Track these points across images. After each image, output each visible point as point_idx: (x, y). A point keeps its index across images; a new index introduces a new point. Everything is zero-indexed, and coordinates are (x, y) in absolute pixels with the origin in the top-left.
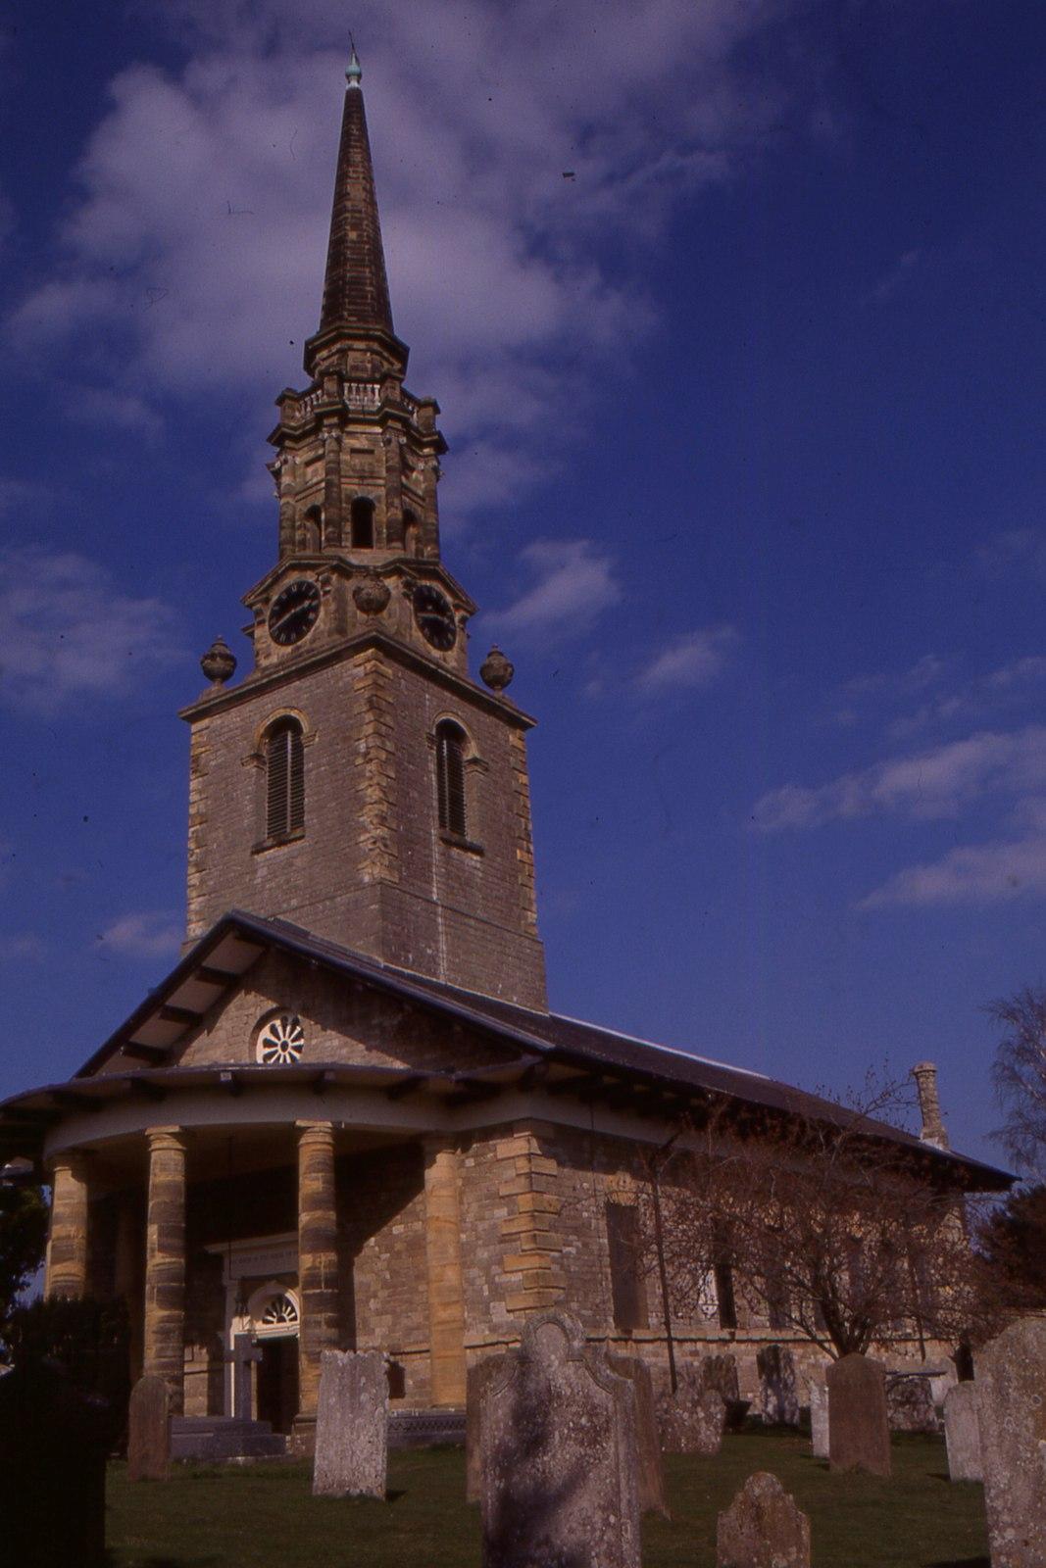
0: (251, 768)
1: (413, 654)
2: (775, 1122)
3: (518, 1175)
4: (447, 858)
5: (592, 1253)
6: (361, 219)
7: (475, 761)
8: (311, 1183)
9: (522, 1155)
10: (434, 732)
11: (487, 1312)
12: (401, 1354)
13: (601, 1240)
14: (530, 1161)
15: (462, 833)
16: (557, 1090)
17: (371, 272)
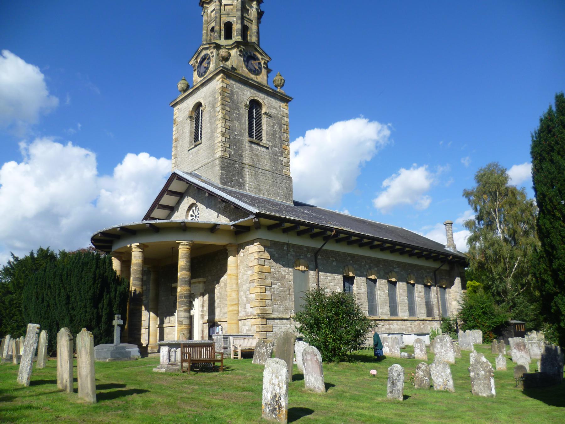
0: (189, 121)
1: (440, 307)
2: (7, 303)
4: (252, 148)
7: (266, 113)
8: (182, 262)
10: (248, 104)
11: (245, 308)
16: (270, 228)
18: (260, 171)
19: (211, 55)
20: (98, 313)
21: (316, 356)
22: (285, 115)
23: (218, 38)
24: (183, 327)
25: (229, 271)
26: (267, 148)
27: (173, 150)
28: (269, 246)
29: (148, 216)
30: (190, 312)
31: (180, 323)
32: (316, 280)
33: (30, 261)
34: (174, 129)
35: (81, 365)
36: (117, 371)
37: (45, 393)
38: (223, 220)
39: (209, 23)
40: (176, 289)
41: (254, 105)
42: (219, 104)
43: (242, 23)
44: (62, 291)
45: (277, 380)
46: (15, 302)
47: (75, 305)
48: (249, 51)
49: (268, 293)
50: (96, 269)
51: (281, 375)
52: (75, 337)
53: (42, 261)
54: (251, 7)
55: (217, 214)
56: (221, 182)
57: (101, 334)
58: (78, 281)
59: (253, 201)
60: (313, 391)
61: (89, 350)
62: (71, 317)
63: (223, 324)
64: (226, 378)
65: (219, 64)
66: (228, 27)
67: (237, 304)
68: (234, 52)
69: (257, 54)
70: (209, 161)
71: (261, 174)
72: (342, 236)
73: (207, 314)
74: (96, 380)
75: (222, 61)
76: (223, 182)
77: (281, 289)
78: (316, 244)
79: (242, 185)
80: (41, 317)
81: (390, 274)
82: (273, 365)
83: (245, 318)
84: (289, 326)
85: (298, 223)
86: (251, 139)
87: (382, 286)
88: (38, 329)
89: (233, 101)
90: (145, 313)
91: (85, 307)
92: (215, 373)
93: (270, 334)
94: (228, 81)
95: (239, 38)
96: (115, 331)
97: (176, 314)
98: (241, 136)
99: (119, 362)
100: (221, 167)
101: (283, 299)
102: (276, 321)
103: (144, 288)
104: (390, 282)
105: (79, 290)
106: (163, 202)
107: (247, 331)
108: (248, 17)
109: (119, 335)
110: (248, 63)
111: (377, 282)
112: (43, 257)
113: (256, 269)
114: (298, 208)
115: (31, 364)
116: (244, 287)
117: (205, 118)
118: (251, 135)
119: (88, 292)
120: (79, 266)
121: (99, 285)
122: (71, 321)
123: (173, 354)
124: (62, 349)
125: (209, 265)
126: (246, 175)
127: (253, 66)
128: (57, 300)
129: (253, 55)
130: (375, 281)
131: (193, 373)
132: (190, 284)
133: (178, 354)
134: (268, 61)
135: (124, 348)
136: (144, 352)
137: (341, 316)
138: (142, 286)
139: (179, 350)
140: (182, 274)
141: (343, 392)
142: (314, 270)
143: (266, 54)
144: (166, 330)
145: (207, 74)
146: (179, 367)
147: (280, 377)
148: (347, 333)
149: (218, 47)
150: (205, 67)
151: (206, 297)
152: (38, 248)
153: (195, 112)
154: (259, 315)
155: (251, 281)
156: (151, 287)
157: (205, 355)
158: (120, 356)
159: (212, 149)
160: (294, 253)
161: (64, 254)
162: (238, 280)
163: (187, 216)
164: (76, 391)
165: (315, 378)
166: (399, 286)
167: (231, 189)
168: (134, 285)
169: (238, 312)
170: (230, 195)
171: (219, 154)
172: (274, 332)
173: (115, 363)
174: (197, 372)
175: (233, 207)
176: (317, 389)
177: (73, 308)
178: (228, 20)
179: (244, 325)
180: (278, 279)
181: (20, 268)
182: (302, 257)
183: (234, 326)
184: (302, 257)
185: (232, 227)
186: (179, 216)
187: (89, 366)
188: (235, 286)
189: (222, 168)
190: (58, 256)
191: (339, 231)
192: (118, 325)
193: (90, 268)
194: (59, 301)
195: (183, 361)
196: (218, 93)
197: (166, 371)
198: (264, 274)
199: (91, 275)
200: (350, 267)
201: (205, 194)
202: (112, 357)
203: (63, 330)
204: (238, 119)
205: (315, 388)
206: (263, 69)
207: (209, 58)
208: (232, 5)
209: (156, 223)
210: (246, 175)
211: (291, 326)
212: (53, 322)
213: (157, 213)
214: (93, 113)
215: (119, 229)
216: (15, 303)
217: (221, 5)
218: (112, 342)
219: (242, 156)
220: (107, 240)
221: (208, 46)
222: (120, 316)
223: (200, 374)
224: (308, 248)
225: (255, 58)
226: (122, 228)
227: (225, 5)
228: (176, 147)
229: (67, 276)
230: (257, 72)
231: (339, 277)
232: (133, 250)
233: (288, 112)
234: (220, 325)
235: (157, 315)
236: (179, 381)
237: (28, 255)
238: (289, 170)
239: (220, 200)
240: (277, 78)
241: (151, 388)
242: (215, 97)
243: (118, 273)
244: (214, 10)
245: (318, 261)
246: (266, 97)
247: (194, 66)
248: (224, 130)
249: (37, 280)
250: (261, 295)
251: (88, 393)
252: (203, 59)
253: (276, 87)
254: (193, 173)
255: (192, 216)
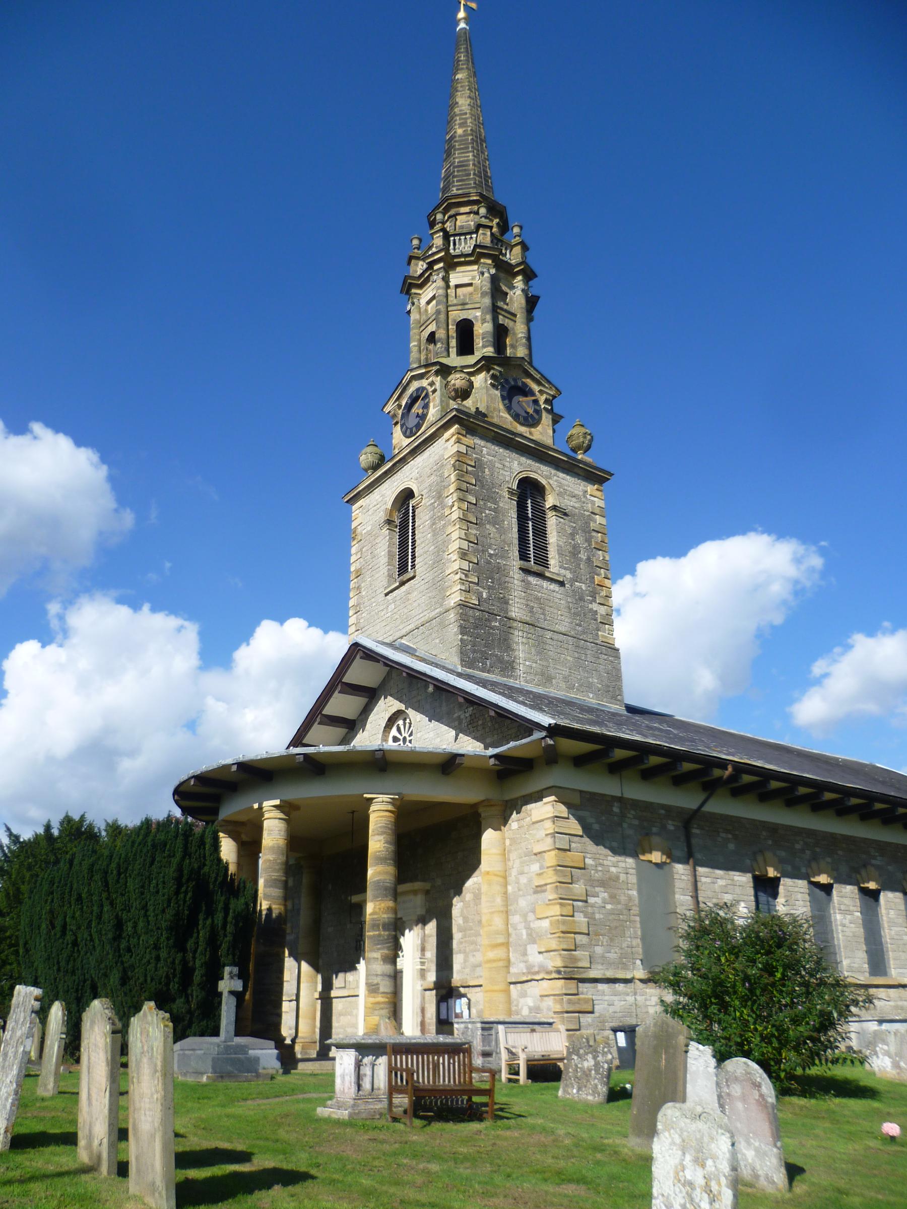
0: (385, 531)
3: (547, 835)
5: (619, 903)
6: (466, 119)
7: (554, 508)
8: (378, 843)
9: (547, 819)
11: (525, 954)
12: (469, 987)
13: (630, 892)
14: (554, 822)
15: (546, 566)
16: (580, 761)
17: (474, 156)
18: (549, 635)
19: (430, 389)
20: (184, 962)
21: (758, 1086)
22: (597, 511)
23: (445, 354)
24: (380, 999)
25: (484, 865)
26: (562, 584)
27: (351, 595)
28: (581, 805)
29: (297, 741)
30: (394, 963)
31: (372, 989)
32: (690, 886)
33: (44, 844)
34: (353, 550)
35: (137, 1105)
36: (230, 1110)
37: (45, 1176)
38: (469, 746)
39: (422, 325)
40: (359, 908)
41: (529, 490)
42: (452, 488)
43: (495, 319)
44: (105, 909)
45: (700, 1173)
46: (8, 934)
47: (133, 941)
48: (512, 378)
49: (580, 918)
50: (183, 859)
51: (714, 1158)
52: (126, 1026)
53: (69, 845)
54: (512, 287)
55: (453, 733)
56: (462, 660)
57: (189, 1012)
58: (143, 887)
59: (538, 701)
60: (751, 1186)
61: (159, 1064)
62: (125, 971)
63: (472, 994)
64: (506, 1139)
65: (448, 405)
66: (465, 330)
67: (507, 945)
68: (481, 380)
69: (529, 381)
70: (433, 614)
71: (549, 641)
72: (747, 778)
73: (433, 967)
74: (177, 1135)
75: (454, 400)
76: (467, 661)
77: (609, 907)
78: (686, 800)
79: (508, 667)
80: (59, 970)
81: (863, 873)
82: (684, 1123)
83: (525, 979)
84: (631, 999)
85: (644, 750)
86: (525, 564)
87: (846, 901)
88: (36, 999)
89: (482, 483)
90: (289, 963)
91: (156, 947)
92: (475, 1126)
93: (586, 1019)
94: (470, 440)
95: (489, 351)
96: (224, 1007)
97: (362, 966)
98: (502, 557)
99: (232, 1084)
100: (461, 626)
101: (615, 931)
102: (601, 987)
103: (290, 906)
104: (865, 892)
105: (145, 908)
106: (330, 709)
107: (530, 1009)
108: (505, 307)
109: (233, 1019)
110: (510, 401)
111: (834, 892)
112: (70, 834)
113: (551, 859)
114: (637, 717)
115: (16, 1093)
116: (523, 903)
117: (423, 520)
118: (524, 556)
119: (163, 911)
120: (145, 850)
121: (190, 895)
122: (124, 980)
123: (366, 1071)
124: (93, 1055)
125: (439, 851)
126: (518, 643)
127: (522, 407)
128: (94, 930)
129: (520, 384)
130: (827, 889)
131: (418, 1122)
132: (395, 895)
133: (379, 1070)
134: (554, 397)
135: (243, 1049)
136: (288, 1058)
137: (779, 975)
138: (286, 898)
139: (383, 1060)
140: (377, 872)
141: (840, 1191)
142: (685, 861)
143: (549, 382)
144: (337, 1006)
145: (423, 429)
146: (383, 1105)
147: (709, 1163)
148: (796, 1021)
149: (445, 371)
150: (418, 416)
151: (431, 927)
152: (61, 816)
153: (399, 511)
154: (559, 972)
155: (539, 889)
156: (304, 901)
157: (447, 1073)
158: (234, 1068)
159: (439, 587)
160: (636, 822)
161: (115, 829)
162: (505, 885)
163: (385, 739)
164: (122, 1169)
165: (757, 1150)
166: (887, 901)
167: (485, 675)
168: (266, 897)
169: (508, 964)
170: (484, 687)
171: (455, 597)
172: (596, 1014)
173: (221, 1085)
174: (429, 1120)
175: (492, 713)
176: (763, 1182)
177: (129, 950)
178: (464, 315)
179: (524, 995)
180: (603, 884)
181: (22, 858)
182: (654, 830)
183: (501, 997)
184: (654, 830)
185: (492, 761)
186: (370, 738)
187: (158, 1107)
188: (499, 900)
189: (463, 630)
190: (104, 833)
191: (741, 769)
192: (232, 993)
193: (169, 856)
194: (100, 932)
195: (392, 1089)
196: (449, 466)
197: (350, 1115)
198: (569, 872)
199: (171, 871)
200: (769, 855)
201: (427, 687)
202: (214, 1072)
203: (96, 1004)
204: (495, 522)
205: (757, 1177)
206: (544, 414)
207: (427, 396)
208: (470, 285)
209: (319, 753)
210: (518, 643)
211: (649, 1003)
212: (85, 981)
213: (318, 731)
214: (187, 556)
215: (234, 768)
216: (10, 937)
217: (448, 287)
218: (216, 1033)
219: (507, 603)
220: (211, 793)
221: (423, 371)
222: (236, 970)
223: (437, 1126)
224: (668, 809)
225: (525, 391)
226: (243, 766)
227: (457, 286)
228: (359, 588)
229: (119, 874)
230: (532, 421)
231: (744, 880)
232: (266, 815)
233: (602, 504)
234: (464, 996)
235: (316, 967)
236: (386, 1147)
237: (41, 831)
238: (611, 632)
239: (461, 700)
240: (574, 431)
241: (318, 1166)
242: (441, 476)
243: (232, 869)
244: (433, 298)
245: (694, 841)
246: (553, 471)
247: (395, 416)
248: (465, 545)
249: (52, 883)
250: (564, 922)
251: (154, 1183)
252: (414, 400)
253: (574, 450)
254: (397, 643)
255: (395, 739)
